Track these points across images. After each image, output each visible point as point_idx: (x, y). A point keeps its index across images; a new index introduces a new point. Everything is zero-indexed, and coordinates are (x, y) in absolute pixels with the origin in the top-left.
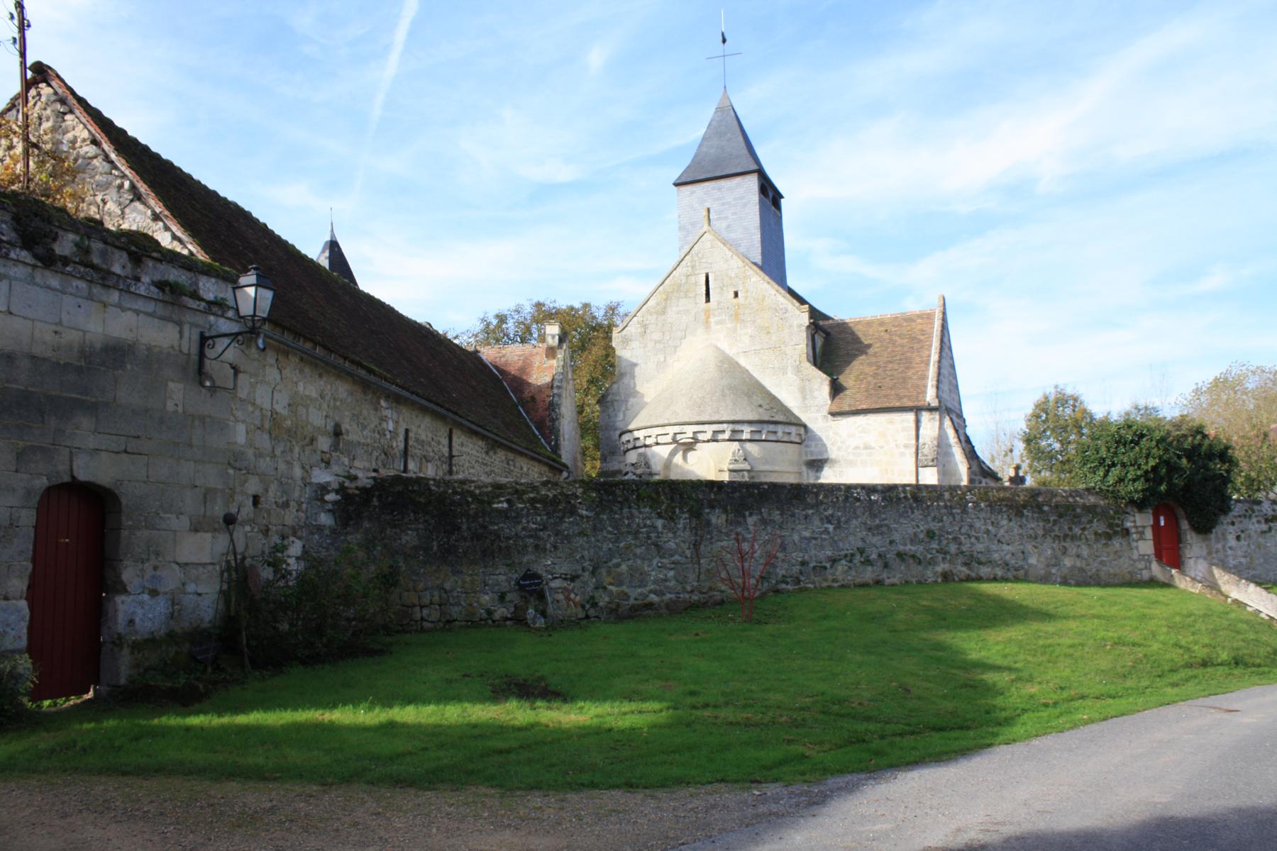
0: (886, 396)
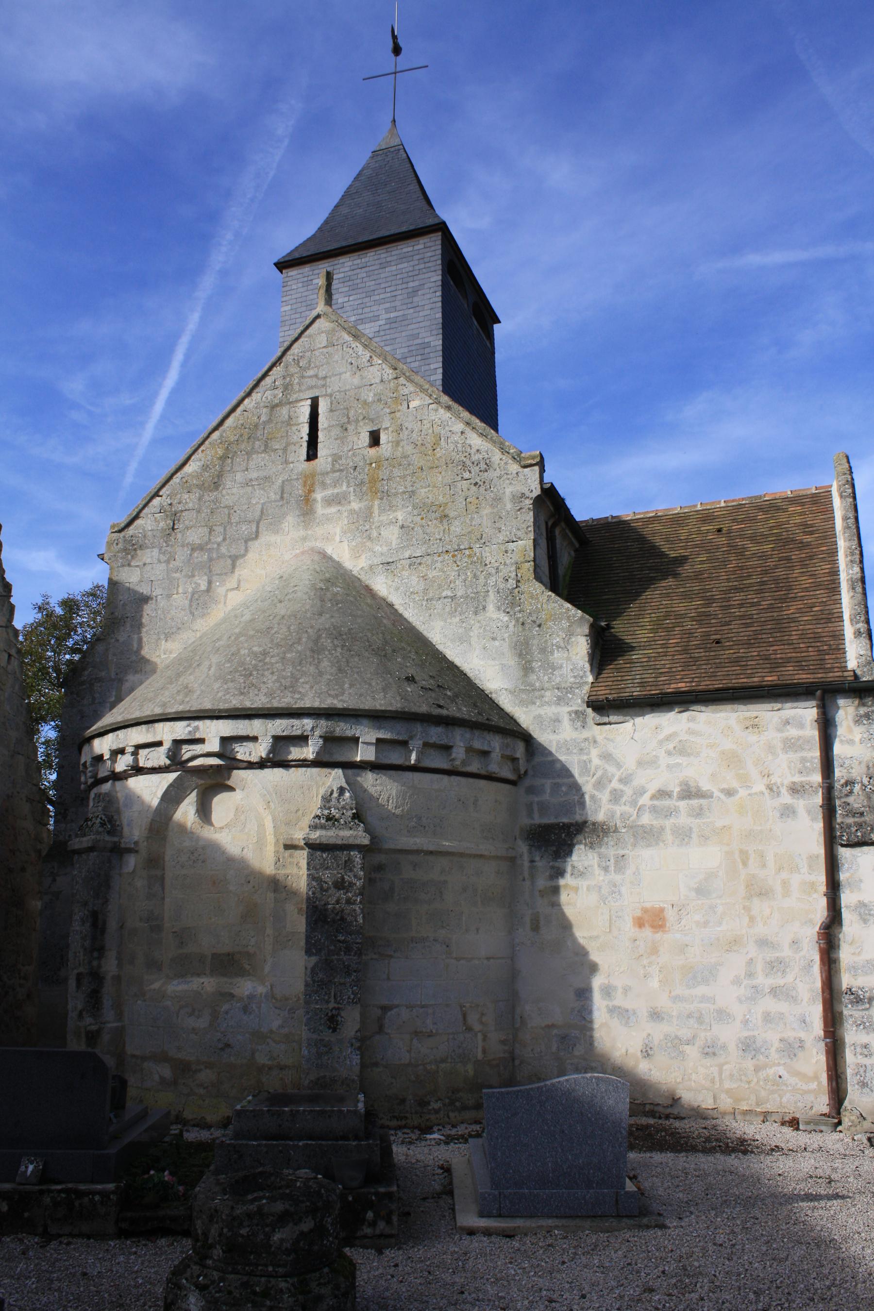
0: (736, 661)
